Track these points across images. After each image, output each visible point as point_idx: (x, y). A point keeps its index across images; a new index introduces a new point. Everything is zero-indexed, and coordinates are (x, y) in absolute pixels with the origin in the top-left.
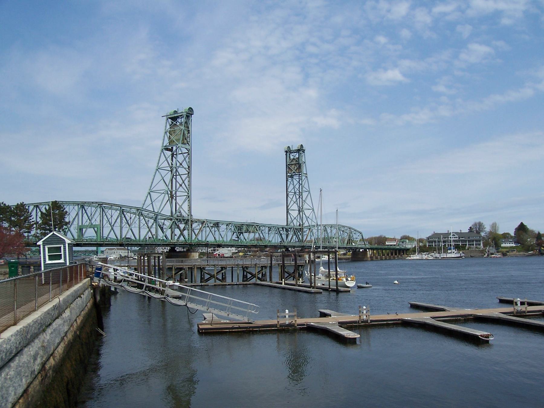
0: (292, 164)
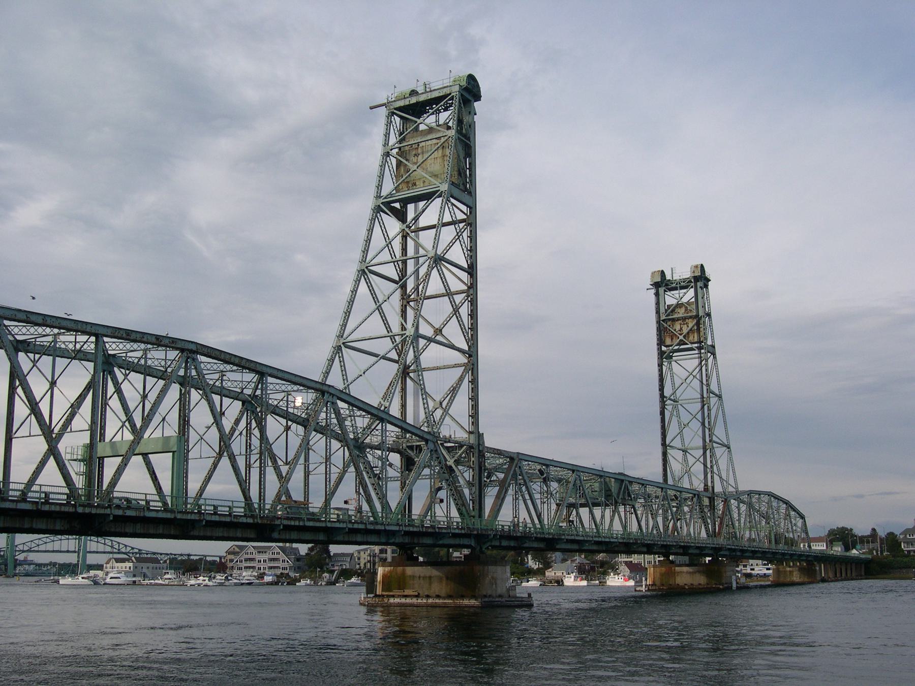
0: (673, 320)
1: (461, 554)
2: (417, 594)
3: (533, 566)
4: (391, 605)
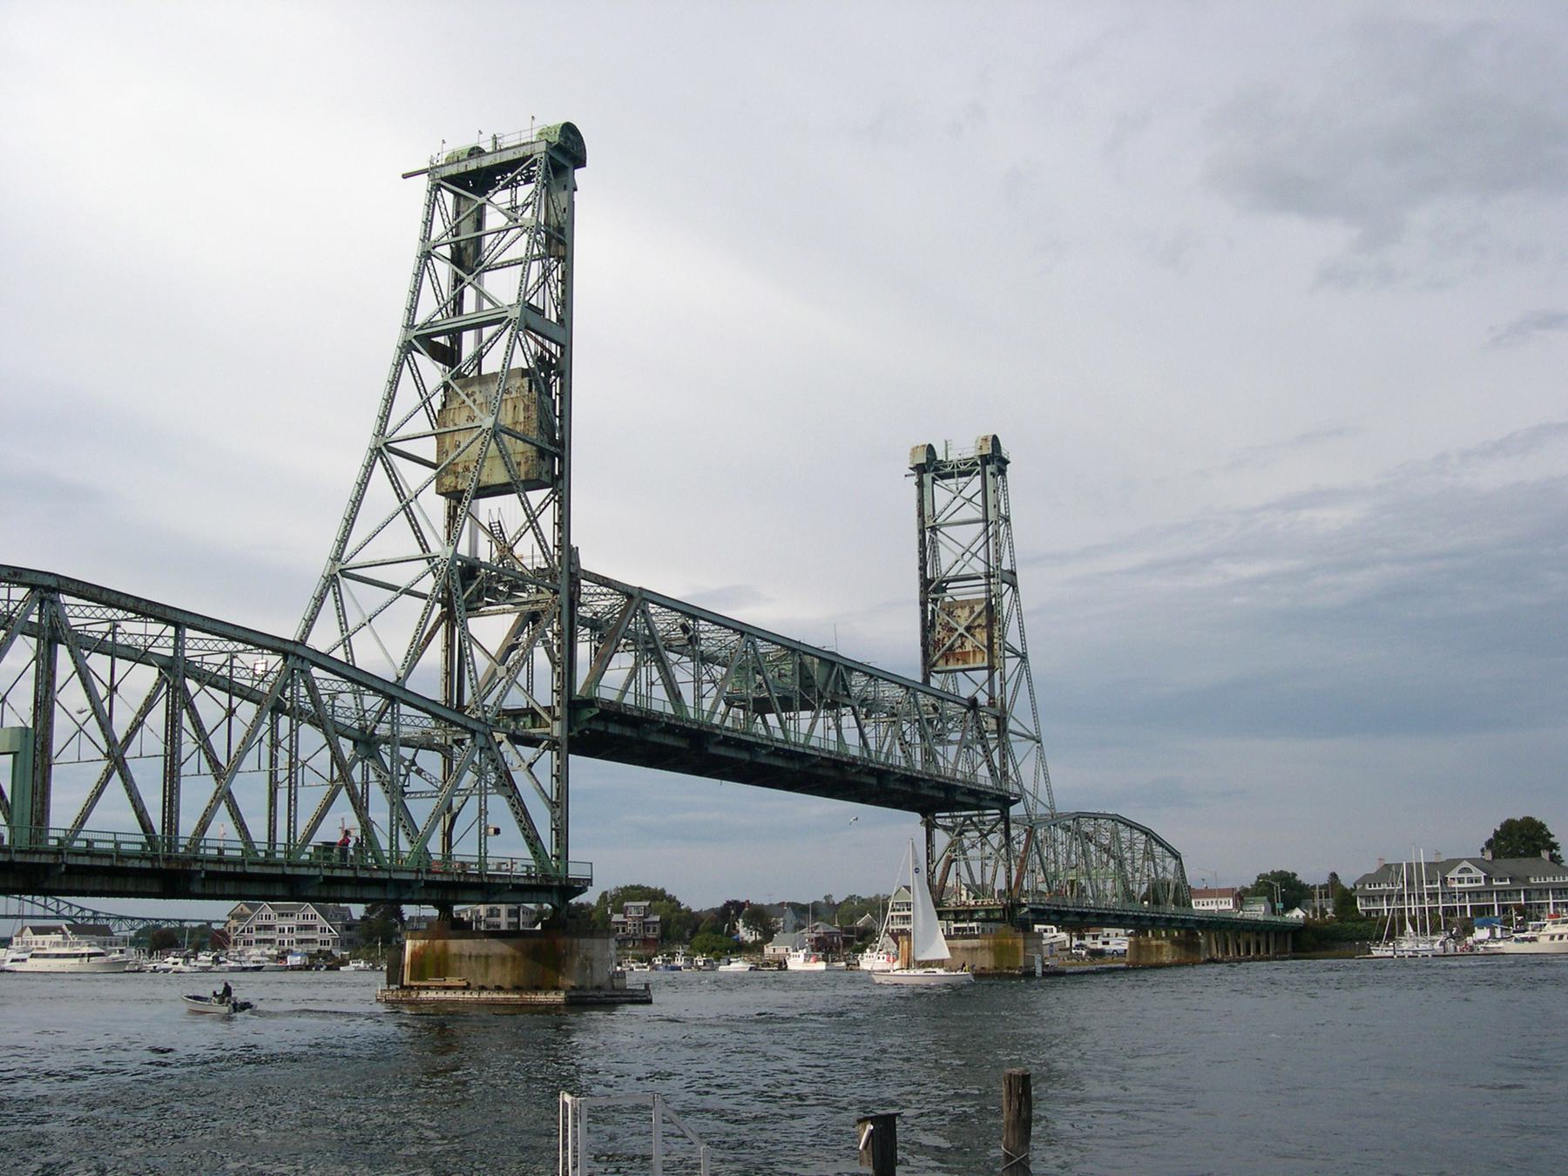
1: (625, 917)
2: (465, 984)
3: (746, 938)
4: (422, 1002)
